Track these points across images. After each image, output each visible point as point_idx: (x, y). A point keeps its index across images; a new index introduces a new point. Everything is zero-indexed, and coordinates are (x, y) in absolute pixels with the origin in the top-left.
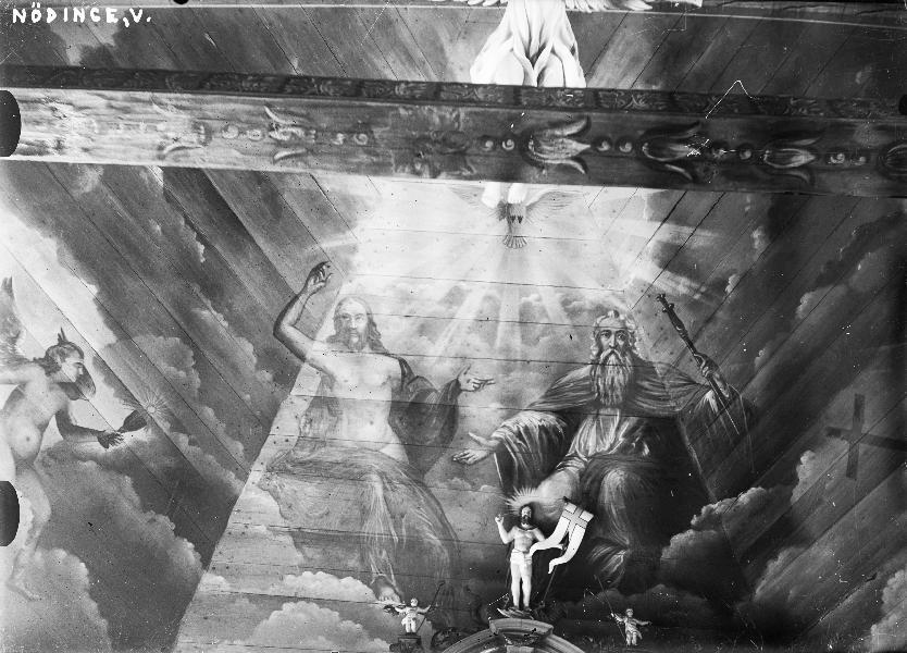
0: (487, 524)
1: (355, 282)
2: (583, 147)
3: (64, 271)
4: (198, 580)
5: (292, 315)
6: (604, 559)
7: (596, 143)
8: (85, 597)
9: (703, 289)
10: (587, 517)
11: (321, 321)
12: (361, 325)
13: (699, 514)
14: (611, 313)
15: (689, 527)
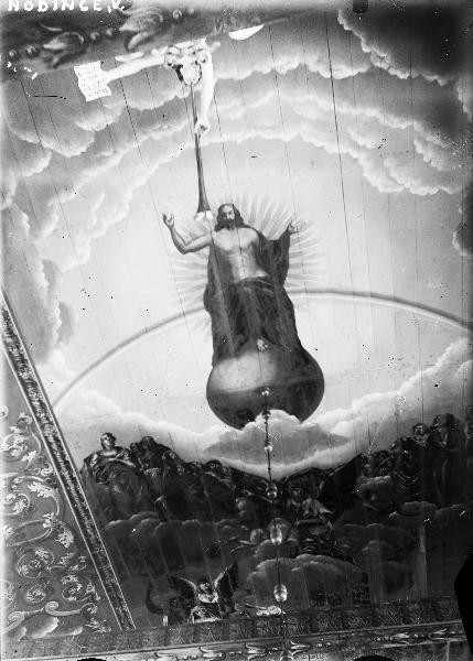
2: (124, 28)
7: (117, 34)
12: (232, 217)
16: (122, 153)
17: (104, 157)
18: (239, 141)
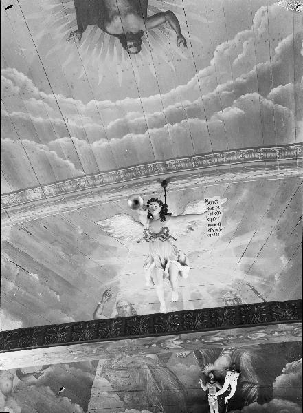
0: (196, 381)
1: (122, 294)
3: (8, 320)
6: (247, 391)
9: (265, 280)
10: (237, 375)
13: (285, 367)
15: (282, 373)
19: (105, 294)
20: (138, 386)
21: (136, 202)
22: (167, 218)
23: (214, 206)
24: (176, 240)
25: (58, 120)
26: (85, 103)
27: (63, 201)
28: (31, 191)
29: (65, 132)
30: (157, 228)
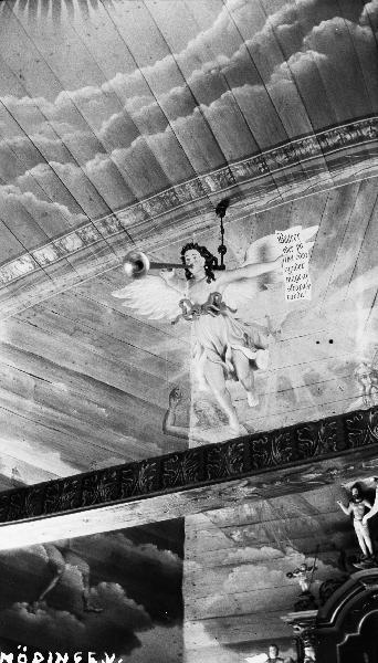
4: (181, 568)
5: (170, 420)
8: (126, 599)
11: (188, 419)
14: (362, 365)
16: (265, 30)
17: (289, 23)
18: (119, 75)
19: (173, 395)
20: (249, 518)
21: (139, 264)
22: (216, 274)
23: (294, 244)
24: (234, 311)
25: (19, 140)
26: (51, 98)
27: (272, 185)
28: (16, 263)
29: (37, 156)
30: (202, 293)
